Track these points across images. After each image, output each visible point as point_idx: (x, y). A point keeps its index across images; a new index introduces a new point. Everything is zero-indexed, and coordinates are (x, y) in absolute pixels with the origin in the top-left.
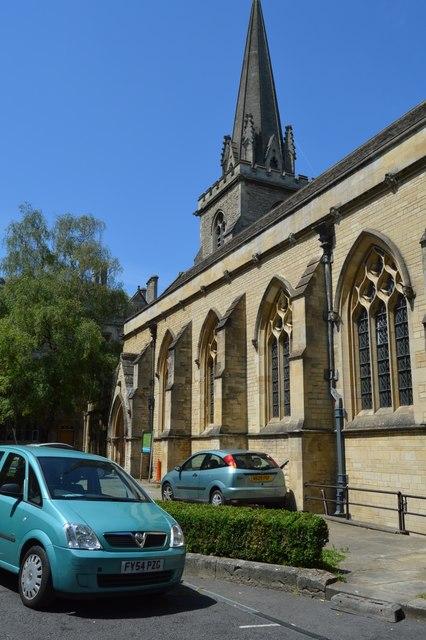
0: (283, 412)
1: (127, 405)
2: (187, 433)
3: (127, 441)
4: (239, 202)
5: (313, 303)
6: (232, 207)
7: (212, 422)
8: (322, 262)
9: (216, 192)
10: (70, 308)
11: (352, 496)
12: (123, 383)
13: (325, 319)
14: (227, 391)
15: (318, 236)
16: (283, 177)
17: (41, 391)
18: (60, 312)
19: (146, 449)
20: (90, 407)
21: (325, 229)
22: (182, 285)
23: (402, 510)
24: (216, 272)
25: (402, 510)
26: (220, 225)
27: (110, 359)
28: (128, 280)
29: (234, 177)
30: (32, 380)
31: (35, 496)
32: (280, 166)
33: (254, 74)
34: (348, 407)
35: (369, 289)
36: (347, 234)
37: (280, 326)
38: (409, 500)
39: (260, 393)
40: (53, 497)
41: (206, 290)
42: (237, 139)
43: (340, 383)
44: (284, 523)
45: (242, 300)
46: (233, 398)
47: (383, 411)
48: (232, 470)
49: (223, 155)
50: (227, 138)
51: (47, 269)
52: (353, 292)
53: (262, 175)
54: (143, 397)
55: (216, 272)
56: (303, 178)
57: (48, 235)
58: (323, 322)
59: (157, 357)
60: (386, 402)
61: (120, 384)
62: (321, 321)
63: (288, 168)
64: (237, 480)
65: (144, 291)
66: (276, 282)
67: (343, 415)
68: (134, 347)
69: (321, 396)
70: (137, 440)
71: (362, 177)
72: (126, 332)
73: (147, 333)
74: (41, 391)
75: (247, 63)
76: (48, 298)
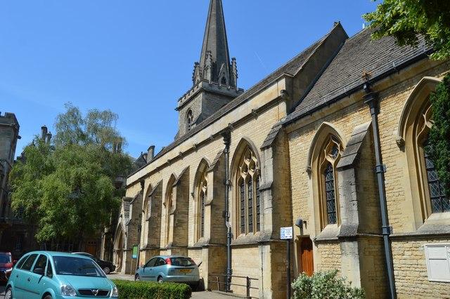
0: (248, 230)
1: (125, 229)
2: (157, 246)
4: (201, 104)
5: (218, 175)
6: (197, 106)
7: (202, 236)
8: (224, 152)
9: (188, 97)
10: (93, 168)
11: (233, 280)
12: (123, 216)
13: (225, 184)
15: (223, 138)
17: (73, 220)
18: (87, 171)
19: (134, 256)
20: (106, 230)
21: (226, 134)
23: (248, 286)
24: (175, 152)
25: (248, 286)
27: (117, 199)
28: (132, 151)
29: (199, 89)
30: (68, 213)
31: (50, 274)
33: (213, 26)
34: (234, 232)
35: (246, 169)
36: (236, 137)
37: (246, 171)
38: (252, 281)
40: (58, 273)
41: (171, 162)
42: (202, 65)
43: (230, 219)
44: (171, 288)
45: (187, 169)
47: (251, 234)
48: (169, 266)
49: (194, 74)
50: (197, 64)
51: (81, 143)
52: (238, 169)
53: (215, 88)
54: (135, 225)
55: (175, 152)
56: (242, 90)
57: (82, 122)
58: (223, 185)
59: (144, 200)
60: (251, 230)
61: (121, 216)
62: (222, 185)
63: (232, 84)
64: (171, 272)
65: (146, 154)
66: (203, 161)
67: (231, 236)
68: (131, 193)
69: (220, 226)
70: (130, 250)
72: (128, 184)
73: (139, 186)
74: (73, 220)
75: (209, 19)
76: (80, 162)
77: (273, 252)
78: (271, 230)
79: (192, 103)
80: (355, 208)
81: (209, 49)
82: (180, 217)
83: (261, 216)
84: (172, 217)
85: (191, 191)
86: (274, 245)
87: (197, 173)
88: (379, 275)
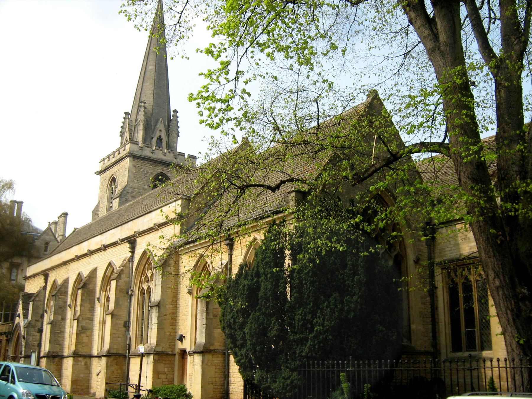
2: (60, 354)
3: (21, 357)
4: (127, 173)
8: (129, 261)
9: (113, 160)
12: (21, 315)
13: (128, 293)
14: (78, 332)
16: (165, 154)
21: (131, 241)
22: (66, 250)
26: (113, 187)
29: (125, 152)
31: (14, 382)
32: (164, 144)
39: (99, 330)
46: (84, 333)
49: (122, 127)
53: (147, 153)
61: (19, 316)
63: (171, 147)
71: (148, 219)
77: (155, 362)
78: (156, 344)
79: (115, 169)
80: (204, 330)
81: (142, 99)
82: (84, 324)
83: (149, 330)
84: (76, 322)
85: (97, 295)
86: (156, 357)
87: (104, 277)
88: (219, 380)
